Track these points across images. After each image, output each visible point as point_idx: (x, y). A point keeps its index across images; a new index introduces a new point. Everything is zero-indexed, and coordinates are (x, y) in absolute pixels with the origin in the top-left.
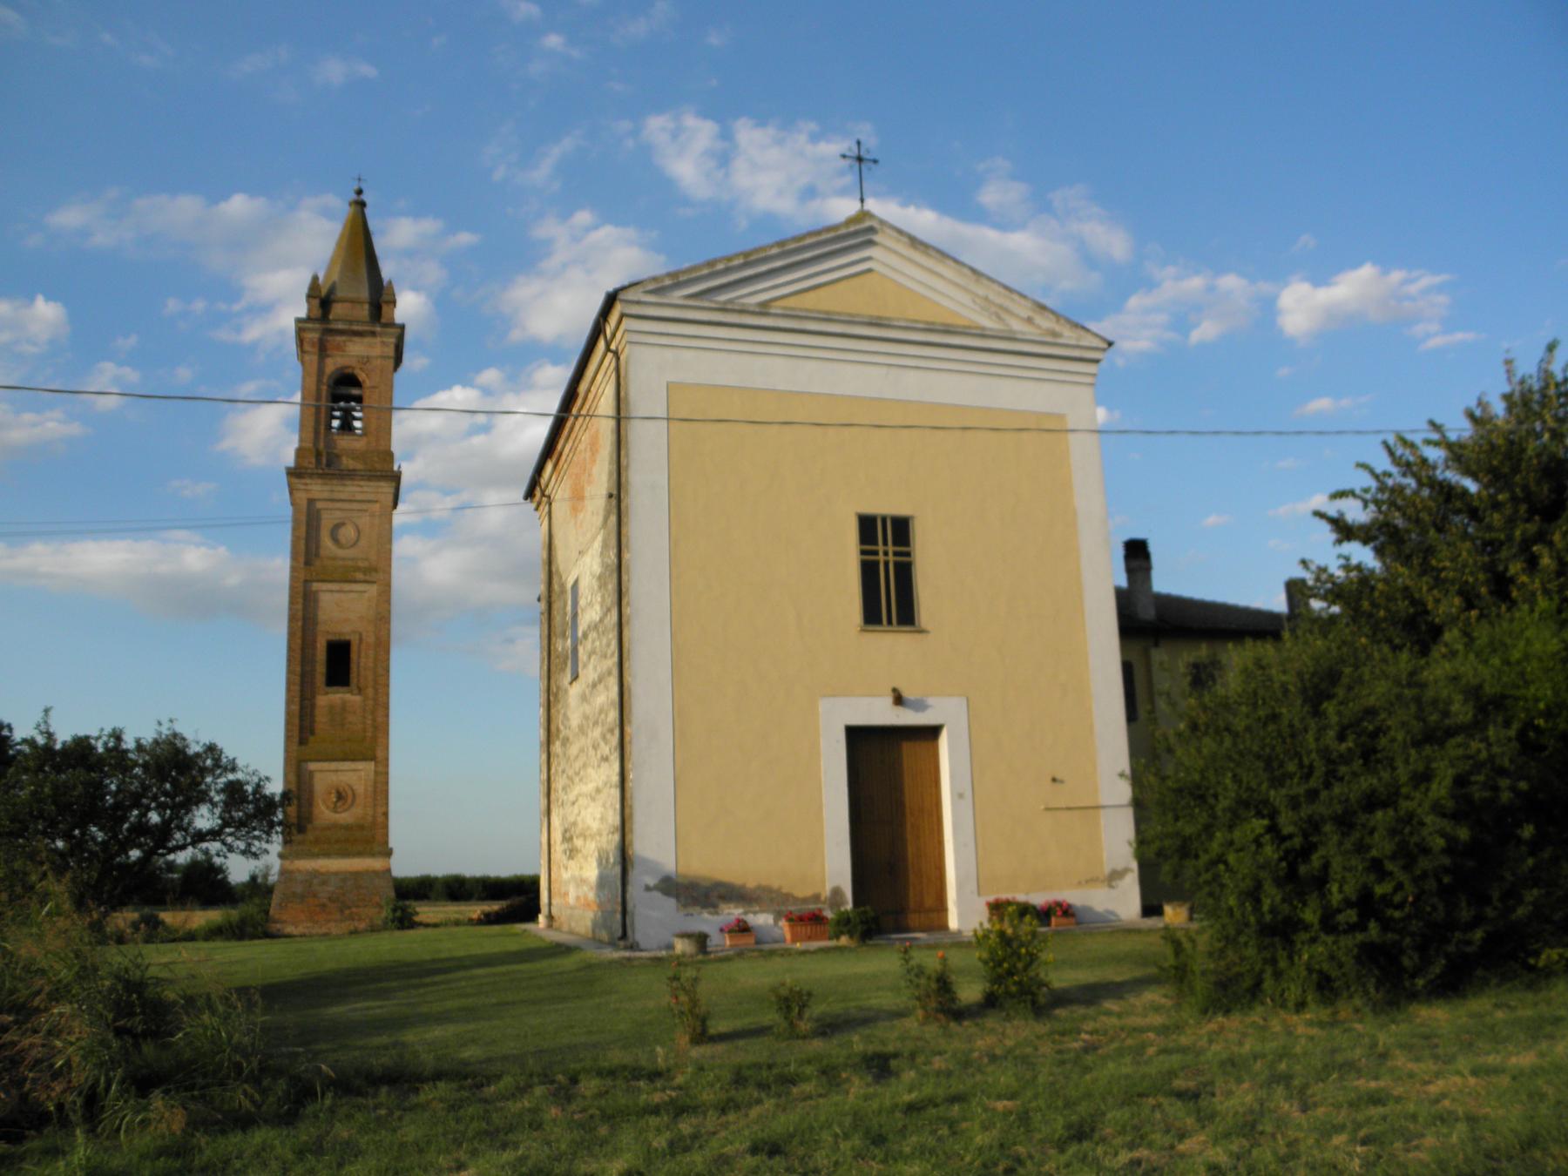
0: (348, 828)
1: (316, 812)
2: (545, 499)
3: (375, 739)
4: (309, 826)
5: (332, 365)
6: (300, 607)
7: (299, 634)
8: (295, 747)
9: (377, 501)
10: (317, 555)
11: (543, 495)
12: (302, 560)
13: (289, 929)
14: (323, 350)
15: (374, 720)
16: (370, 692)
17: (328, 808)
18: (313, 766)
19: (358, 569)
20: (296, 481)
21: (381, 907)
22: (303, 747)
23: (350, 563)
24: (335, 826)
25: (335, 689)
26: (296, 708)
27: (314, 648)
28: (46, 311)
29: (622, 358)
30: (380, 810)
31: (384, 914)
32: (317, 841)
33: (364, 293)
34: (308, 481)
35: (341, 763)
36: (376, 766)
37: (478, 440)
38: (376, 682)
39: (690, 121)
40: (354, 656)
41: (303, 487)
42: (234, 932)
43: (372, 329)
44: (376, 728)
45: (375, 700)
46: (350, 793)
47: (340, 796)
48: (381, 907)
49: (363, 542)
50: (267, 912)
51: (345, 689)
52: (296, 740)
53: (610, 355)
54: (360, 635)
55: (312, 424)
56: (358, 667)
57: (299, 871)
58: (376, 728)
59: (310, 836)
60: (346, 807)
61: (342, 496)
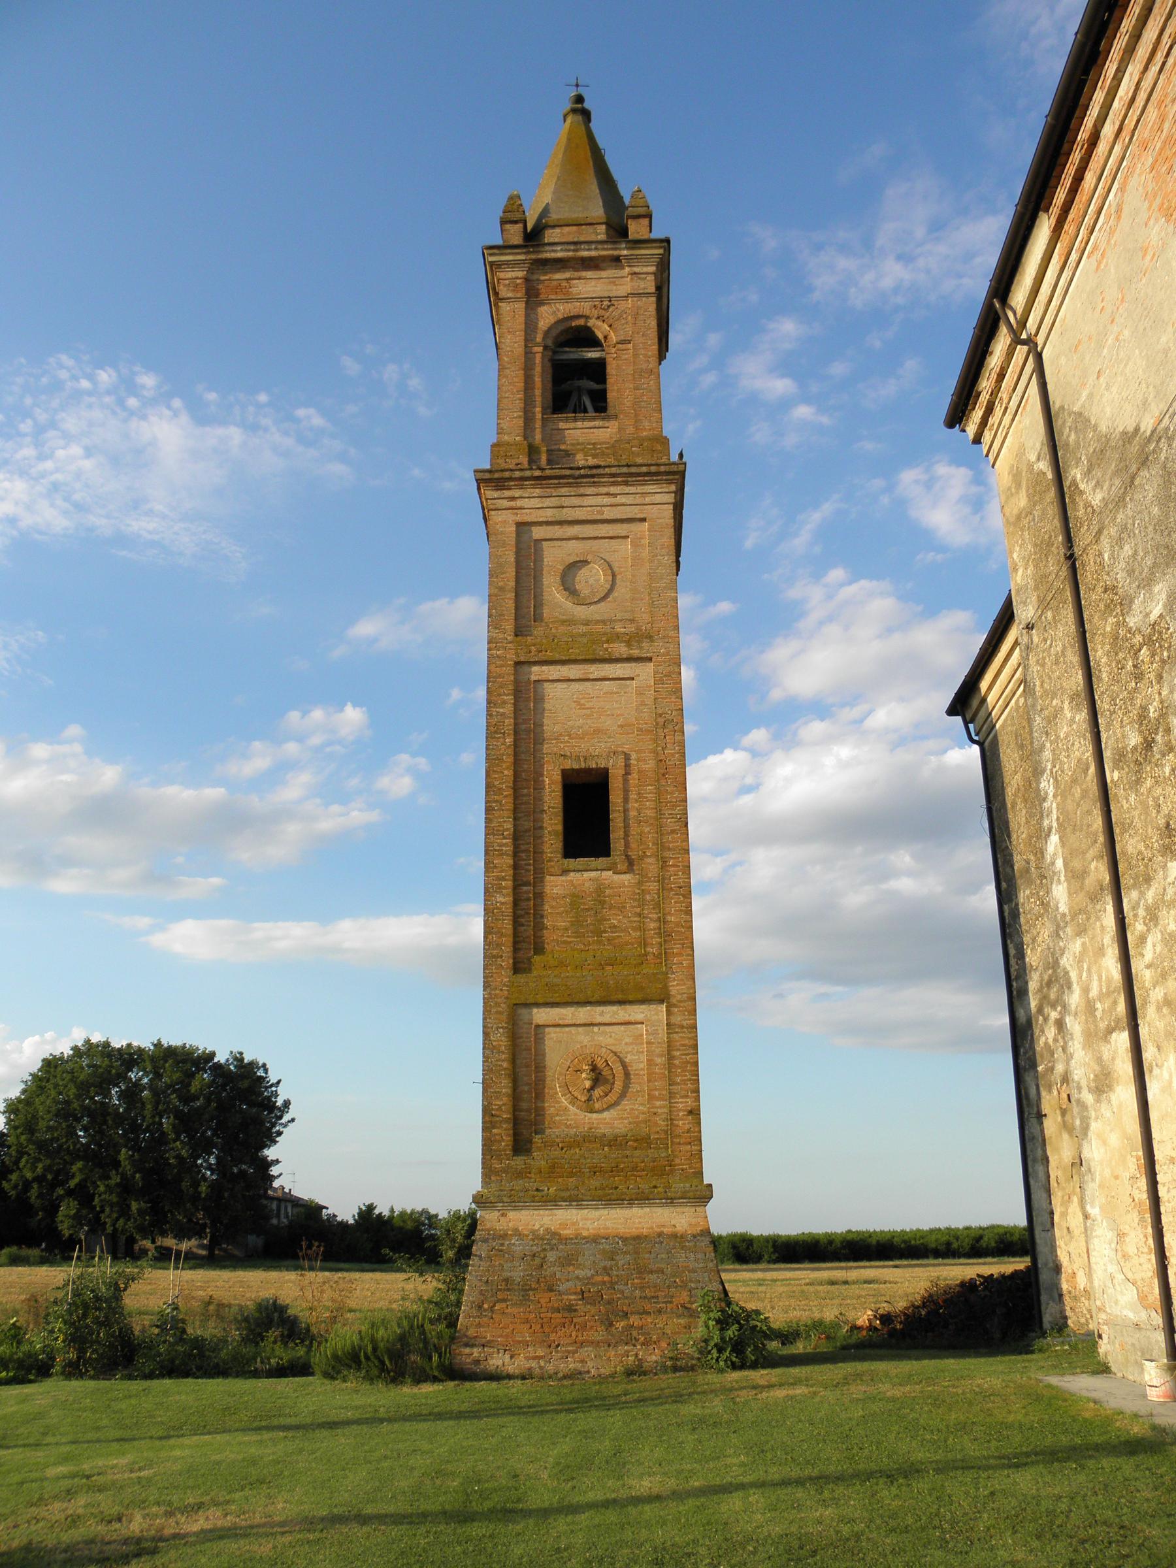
0: (615, 1142)
1: (550, 1109)
2: (1021, 350)
3: (664, 956)
4: (537, 1139)
5: (547, 316)
6: (508, 709)
7: (508, 760)
8: (505, 976)
9: (644, 520)
10: (538, 618)
11: (1017, 341)
12: (509, 626)
13: (497, 1361)
14: (532, 297)
15: (662, 920)
16: (651, 865)
17: (574, 1100)
18: (541, 1015)
19: (616, 637)
20: (490, 494)
21: (693, 1314)
22: (521, 979)
23: (599, 628)
24: (589, 1139)
25: (581, 861)
26: (504, 899)
27: (538, 786)
28: (353, 716)
29: (1046, 355)
30: (682, 1104)
31: (699, 1332)
32: (553, 1170)
33: (597, 210)
34: (517, 493)
35: (599, 1009)
36: (669, 1013)
37: (747, 800)
38: (661, 846)
39: (942, 470)
40: (615, 797)
41: (506, 504)
42: (382, 1363)
43: (616, 253)
44: (665, 934)
45: (662, 880)
46: (618, 1069)
47: (598, 1077)
48: (693, 1314)
49: (621, 592)
50: (452, 1322)
51: (602, 861)
52: (507, 961)
53: (1021, 350)
54: (627, 757)
55: (520, 404)
56: (626, 819)
57: (517, 1233)
58: (665, 934)
59: (539, 1159)
60: (612, 1098)
61: (580, 514)
